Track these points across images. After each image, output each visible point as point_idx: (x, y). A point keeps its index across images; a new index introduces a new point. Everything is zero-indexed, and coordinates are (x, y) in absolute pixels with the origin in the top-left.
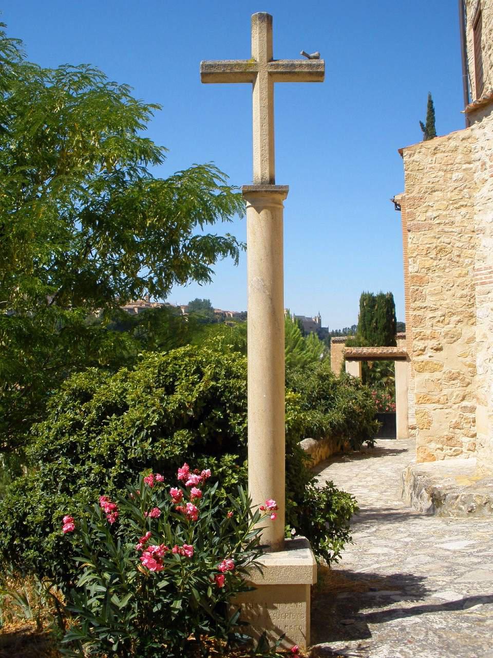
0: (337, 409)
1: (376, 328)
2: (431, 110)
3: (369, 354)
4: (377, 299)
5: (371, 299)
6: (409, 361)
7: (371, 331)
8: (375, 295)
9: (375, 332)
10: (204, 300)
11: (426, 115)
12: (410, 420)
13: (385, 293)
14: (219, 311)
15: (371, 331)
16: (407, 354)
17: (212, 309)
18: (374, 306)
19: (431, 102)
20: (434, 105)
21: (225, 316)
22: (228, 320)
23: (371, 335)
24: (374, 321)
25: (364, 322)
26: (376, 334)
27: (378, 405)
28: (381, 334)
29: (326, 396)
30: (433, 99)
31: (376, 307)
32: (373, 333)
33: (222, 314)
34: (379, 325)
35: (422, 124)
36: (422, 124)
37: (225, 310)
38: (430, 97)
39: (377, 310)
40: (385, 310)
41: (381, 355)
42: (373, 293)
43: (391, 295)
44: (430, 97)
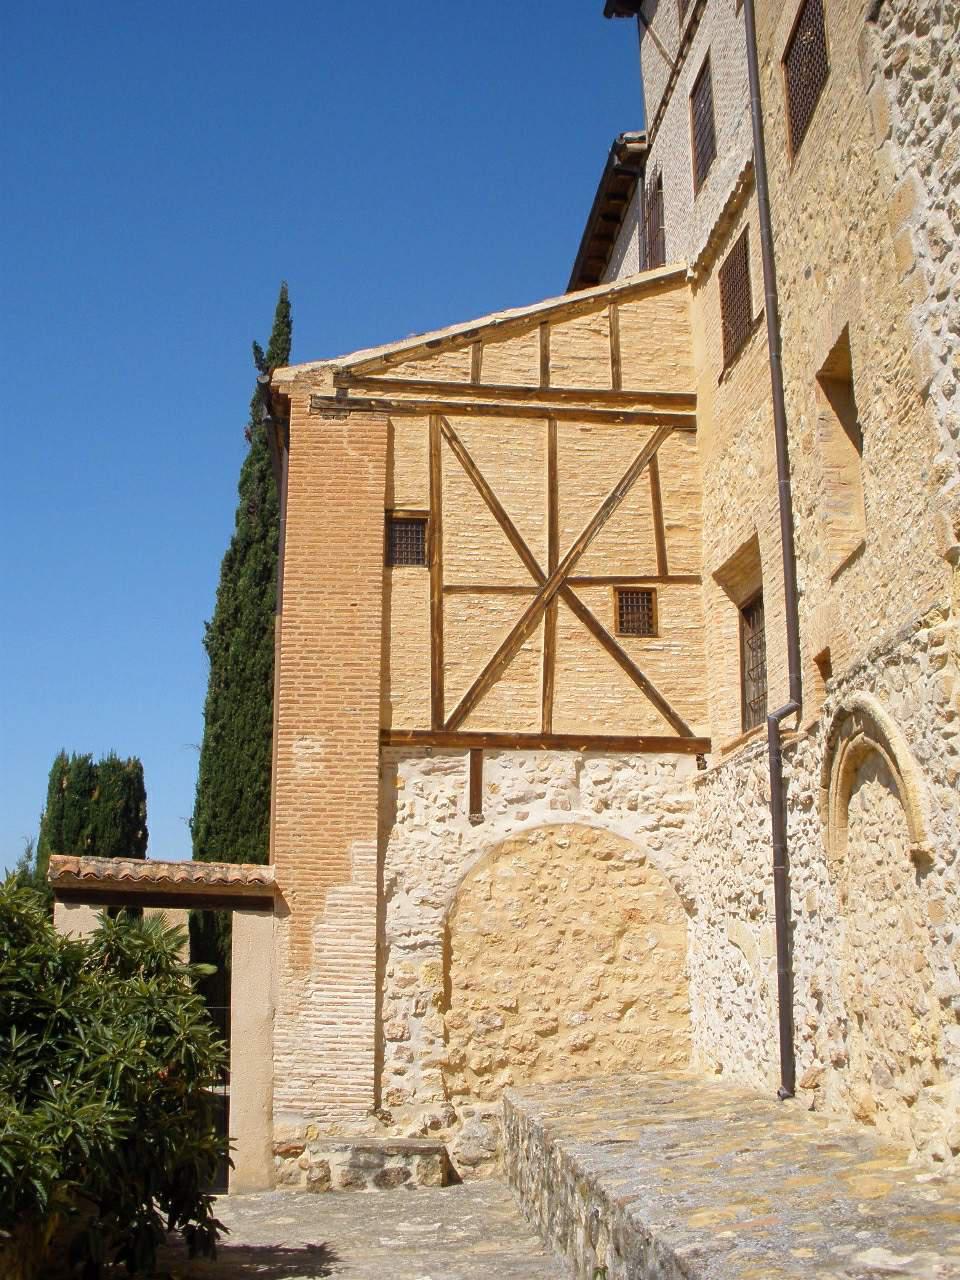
0: (85, 1077)
2: (284, 322)
3: (145, 880)
5: (84, 771)
6: (284, 912)
8: (95, 761)
11: (269, 334)
12: (279, 1123)
13: (123, 759)
16: (277, 889)
18: (89, 792)
19: (285, 304)
20: (293, 313)
24: (88, 831)
25: (60, 833)
29: (29, 1015)
30: (291, 299)
35: (257, 350)
36: (257, 350)
38: (284, 292)
39: (97, 802)
40: (121, 804)
41: (184, 890)
42: (90, 756)
43: (138, 769)
44: (284, 292)
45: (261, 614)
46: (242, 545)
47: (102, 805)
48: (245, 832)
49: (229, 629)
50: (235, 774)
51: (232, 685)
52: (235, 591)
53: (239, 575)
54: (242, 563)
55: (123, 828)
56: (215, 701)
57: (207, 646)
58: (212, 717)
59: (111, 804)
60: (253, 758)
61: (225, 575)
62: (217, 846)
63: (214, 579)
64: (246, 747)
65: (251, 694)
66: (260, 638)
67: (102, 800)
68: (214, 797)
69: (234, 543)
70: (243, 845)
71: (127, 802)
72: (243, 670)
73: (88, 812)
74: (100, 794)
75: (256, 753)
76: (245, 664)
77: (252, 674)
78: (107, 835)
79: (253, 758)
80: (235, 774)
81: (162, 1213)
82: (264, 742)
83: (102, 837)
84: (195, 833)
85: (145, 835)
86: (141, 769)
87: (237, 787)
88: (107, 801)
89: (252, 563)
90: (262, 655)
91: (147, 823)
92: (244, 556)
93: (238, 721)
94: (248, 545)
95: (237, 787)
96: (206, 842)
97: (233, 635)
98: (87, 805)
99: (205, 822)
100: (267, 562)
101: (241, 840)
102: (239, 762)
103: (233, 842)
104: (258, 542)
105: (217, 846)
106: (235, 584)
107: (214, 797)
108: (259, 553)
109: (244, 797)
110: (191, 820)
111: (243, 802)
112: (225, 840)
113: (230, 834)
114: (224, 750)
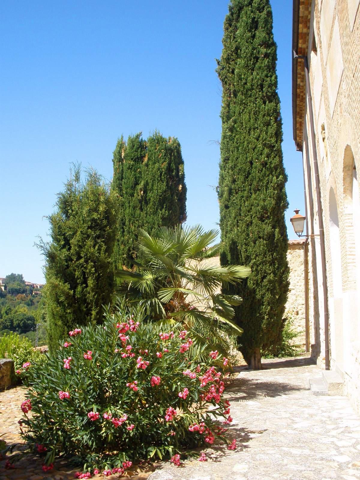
1: (145, 201)
4: (148, 145)
7: (134, 208)
9: (141, 209)
10: (18, 274)
14: (29, 284)
15: (134, 208)
17: (24, 282)
18: (142, 157)
21: (34, 287)
22: (36, 290)
23: (133, 215)
24: (141, 185)
26: (143, 214)
27: (144, 375)
28: (155, 213)
31: (146, 159)
32: (138, 212)
33: (32, 286)
34: (150, 194)
37: (33, 283)
39: (147, 165)
40: (165, 165)
42: (140, 134)
43: (178, 146)
45: (254, 49)
46: (235, 10)
47: (150, 166)
48: (257, 190)
49: (233, 60)
50: (246, 151)
51: (239, 94)
52: (234, 38)
53: (236, 28)
54: (237, 21)
55: (167, 182)
56: (228, 106)
57: (219, 75)
58: (226, 117)
59: (157, 165)
60: (258, 140)
61: (227, 29)
62: (237, 201)
63: (220, 32)
64: (252, 133)
65: (252, 99)
66: (254, 64)
67: (150, 163)
68: (232, 169)
69: (231, 9)
70: (255, 199)
71: (169, 164)
72: (246, 84)
73: (140, 172)
74: (149, 159)
75: (259, 136)
76: (246, 80)
77: (252, 86)
78: (155, 188)
79: (258, 140)
80: (246, 151)
81: (14, 453)
82: (265, 128)
83: (152, 189)
84: (221, 196)
85: (184, 189)
86: (179, 145)
87: (248, 159)
88: (155, 163)
89: (244, 18)
90: (258, 74)
91: (186, 181)
92: (239, 16)
93: (245, 117)
94: (241, 9)
95: (248, 159)
96: (229, 200)
97: (236, 63)
98: (140, 168)
99: (227, 186)
100: (254, 18)
101: (253, 196)
102: (248, 143)
103: (248, 197)
104: (247, 6)
105: (237, 201)
106: (234, 34)
107: (232, 169)
108: (249, 12)
109: (253, 166)
110: (217, 188)
111: (254, 170)
112: (242, 197)
113: (246, 192)
114: (237, 137)
